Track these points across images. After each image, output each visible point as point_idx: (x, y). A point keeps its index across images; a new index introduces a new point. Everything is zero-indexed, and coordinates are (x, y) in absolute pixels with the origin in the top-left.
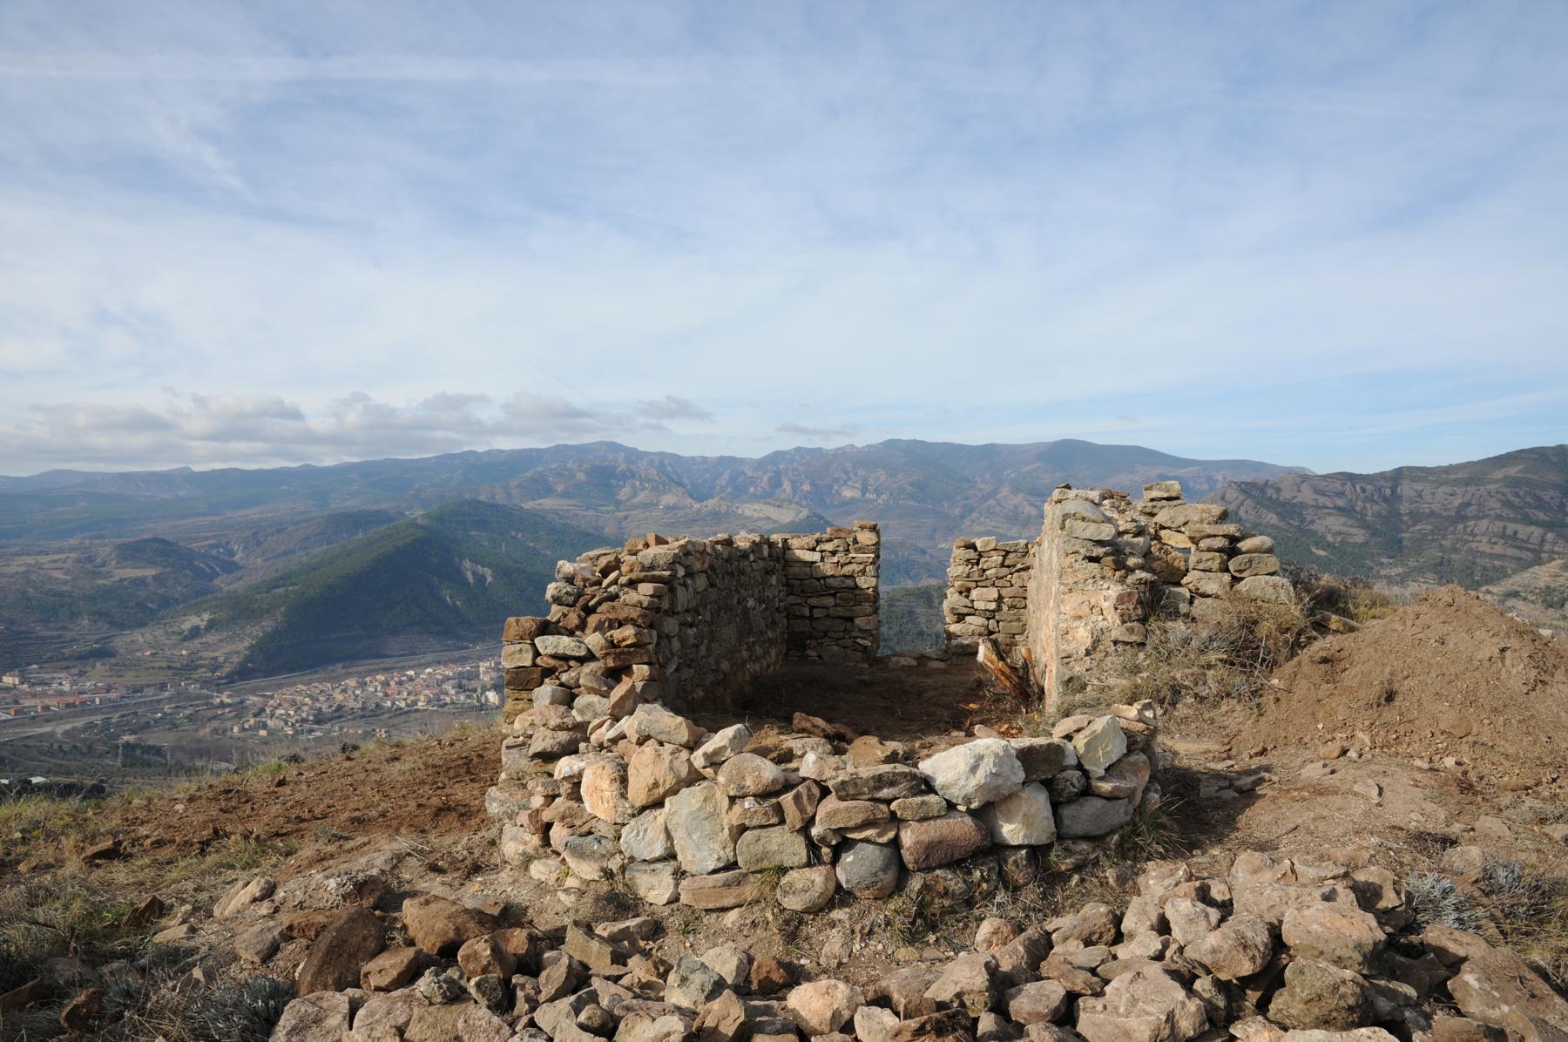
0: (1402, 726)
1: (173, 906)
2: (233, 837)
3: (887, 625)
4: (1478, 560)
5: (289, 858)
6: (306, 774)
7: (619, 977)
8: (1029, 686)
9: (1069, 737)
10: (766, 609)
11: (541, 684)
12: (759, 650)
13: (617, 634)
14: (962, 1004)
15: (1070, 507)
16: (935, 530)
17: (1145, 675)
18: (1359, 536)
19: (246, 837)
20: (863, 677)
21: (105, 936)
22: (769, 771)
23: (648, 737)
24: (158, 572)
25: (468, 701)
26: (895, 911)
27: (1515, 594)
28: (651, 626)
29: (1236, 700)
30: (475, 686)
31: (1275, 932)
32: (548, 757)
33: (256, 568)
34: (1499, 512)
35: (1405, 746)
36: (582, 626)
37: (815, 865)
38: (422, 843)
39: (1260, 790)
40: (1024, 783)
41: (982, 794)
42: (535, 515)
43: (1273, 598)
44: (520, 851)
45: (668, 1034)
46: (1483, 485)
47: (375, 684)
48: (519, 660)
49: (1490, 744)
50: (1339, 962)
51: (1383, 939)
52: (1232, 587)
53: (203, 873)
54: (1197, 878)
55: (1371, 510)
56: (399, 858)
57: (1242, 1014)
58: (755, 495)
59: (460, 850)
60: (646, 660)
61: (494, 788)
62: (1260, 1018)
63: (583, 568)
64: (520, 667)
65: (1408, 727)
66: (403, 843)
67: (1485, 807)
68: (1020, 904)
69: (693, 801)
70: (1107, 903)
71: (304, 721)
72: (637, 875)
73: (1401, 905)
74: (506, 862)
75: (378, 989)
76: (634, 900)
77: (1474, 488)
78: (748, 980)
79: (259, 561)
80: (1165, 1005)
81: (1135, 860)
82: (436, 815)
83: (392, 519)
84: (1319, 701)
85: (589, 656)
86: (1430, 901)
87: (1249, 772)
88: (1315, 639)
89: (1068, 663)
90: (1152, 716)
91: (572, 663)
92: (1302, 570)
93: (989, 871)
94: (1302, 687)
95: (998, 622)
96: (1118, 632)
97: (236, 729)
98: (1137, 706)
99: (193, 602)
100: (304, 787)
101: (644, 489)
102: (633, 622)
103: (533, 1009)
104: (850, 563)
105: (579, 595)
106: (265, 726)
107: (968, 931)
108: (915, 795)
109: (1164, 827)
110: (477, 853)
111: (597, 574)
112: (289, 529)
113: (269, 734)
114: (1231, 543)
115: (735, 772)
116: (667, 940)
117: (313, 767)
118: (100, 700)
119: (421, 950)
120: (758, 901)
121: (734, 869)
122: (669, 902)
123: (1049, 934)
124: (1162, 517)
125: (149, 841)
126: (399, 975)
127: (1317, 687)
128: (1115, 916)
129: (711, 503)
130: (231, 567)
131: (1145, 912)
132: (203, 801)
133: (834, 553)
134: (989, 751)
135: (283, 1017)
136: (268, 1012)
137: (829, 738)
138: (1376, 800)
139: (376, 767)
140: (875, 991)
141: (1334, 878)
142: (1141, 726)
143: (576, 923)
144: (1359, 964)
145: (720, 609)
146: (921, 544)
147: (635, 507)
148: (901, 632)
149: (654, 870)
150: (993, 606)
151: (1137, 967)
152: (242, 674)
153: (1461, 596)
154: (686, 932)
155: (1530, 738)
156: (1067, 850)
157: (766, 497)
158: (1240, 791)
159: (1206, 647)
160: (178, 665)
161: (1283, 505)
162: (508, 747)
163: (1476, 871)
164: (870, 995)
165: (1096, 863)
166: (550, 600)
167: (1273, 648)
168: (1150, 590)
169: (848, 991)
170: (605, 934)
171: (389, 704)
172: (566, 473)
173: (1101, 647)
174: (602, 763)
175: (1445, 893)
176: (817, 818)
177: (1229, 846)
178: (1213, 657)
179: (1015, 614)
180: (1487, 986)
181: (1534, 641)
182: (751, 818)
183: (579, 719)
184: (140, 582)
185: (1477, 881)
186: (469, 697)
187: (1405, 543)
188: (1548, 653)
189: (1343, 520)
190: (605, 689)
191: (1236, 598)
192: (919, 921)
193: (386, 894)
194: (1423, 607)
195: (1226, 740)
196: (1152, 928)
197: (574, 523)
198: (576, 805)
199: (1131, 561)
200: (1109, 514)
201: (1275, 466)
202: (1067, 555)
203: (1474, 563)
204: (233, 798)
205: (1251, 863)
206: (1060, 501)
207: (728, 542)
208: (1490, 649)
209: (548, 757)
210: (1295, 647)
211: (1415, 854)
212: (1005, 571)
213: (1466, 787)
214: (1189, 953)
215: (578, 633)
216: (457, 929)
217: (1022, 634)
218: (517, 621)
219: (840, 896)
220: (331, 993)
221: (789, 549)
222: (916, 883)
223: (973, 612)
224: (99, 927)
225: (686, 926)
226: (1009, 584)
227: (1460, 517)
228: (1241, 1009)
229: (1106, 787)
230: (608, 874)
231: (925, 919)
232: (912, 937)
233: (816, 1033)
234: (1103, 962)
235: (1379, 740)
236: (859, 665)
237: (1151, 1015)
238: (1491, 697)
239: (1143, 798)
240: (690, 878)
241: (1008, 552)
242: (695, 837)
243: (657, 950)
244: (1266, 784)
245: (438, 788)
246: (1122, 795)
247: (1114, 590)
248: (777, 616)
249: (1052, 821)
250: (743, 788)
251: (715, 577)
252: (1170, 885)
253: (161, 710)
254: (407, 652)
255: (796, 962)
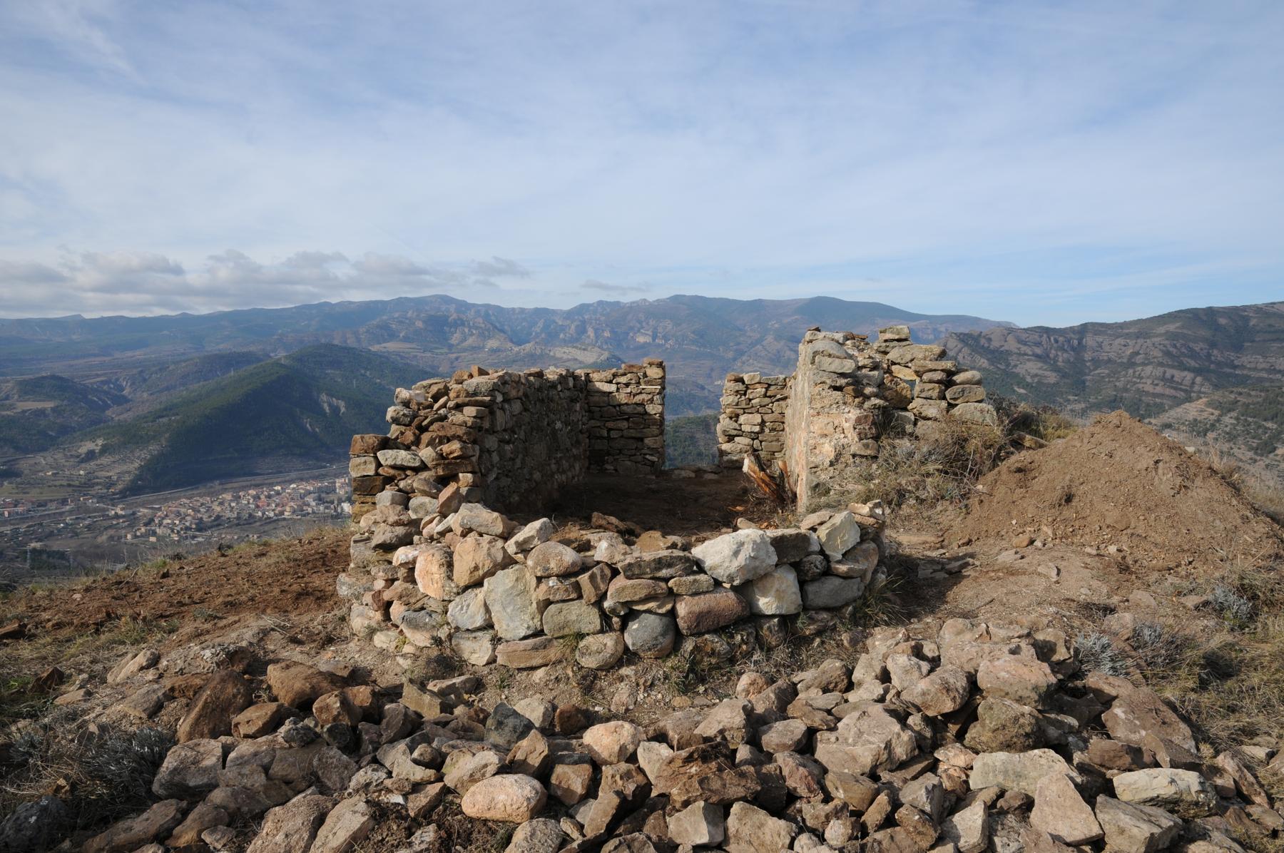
0: (1077, 522)
1: (71, 675)
2: (123, 619)
3: (672, 448)
4: (1143, 398)
5: (171, 635)
6: (187, 568)
7: (447, 723)
8: (785, 491)
9: (814, 529)
10: (572, 430)
11: (383, 489)
12: (565, 464)
13: (446, 448)
14: (724, 738)
15: (819, 345)
16: (712, 370)
17: (877, 481)
18: (1052, 378)
19: (134, 619)
20: (650, 486)
21: (13, 701)
22: (569, 556)
23: (471, 530)
24: (57, 404)
25: (327, 511)
26: (672, 667)
27: (1168, 426)
28: (474, 442)
29: (948, 502)
30: (332, 498)
31: (972, 680)
32: (388, 548)
33: (143, 402)
34: (1160, 360)
35: (1079, 537)
36: (417, 442)
37: (607, 632)
38: (284, 621)
39: (965, 572)
40: (777, 565)
41: (743, 574)
42: (381, 356)
43: (981, 420)
44: (366, 625)
45: (486, 766)
46: (1149, 338)
47: (248, 497)
48: (364, 470)
49: (1144, 535)
50: (1020, 700)
51: (1054, 682)
52: (948, 412)
53: (98, 648)
54: (913, 640)
55: (1062, 357)
56: (264, 633)
57: (944, 742)
58: (564, 340)
59: (316, 626)
60: (470, 470)
61: (344, 575)
62: (958, 745)
63: (418, 394)
64: (364, 476)
65: (1082, 522)
66: (268, 621)
67: (1138, 583)
68: (772, 662)
69: (507, 581)
70: (842, 660)
71: (188, 529)
72: (462, 642)
73: (1070, 658)
74: (354, 635)
75: (247, 736)
76: (459, 661)
77: (1142, 340)
78: (552, 724)
79: (145, 395)
80: (884, 736)
81: (865, 626)
82: (297, 599)
83: (259, 360)
84: (1014, 502)
85: (423, 466)
86: (1092, 654)
87: (957, 559)
88: (1012, 453)
89: (815, 472)
90: (881, 513)
91: (408, 472)
92: (1004, 399)
93: (748, 635)
94: (1001, 491)
95: (761, 442)
96: (856, 448)
97: (129, 536)
98: (870, 505)
99: (88, 430)
100: (185, 578)
101: (472, 334)
102: (459, 438)
103: (376, 749)
104: (641, 393)
105: (415, 416)
106: (154, 533)
107: (731, 683)
108: (688, 575)
109: (889, 601)
110: (330, 628)
111: (430, 399)
112: (170, 368)
113: (158, 540)
114: (948, 376)
115: (541, 557)
116: (486, 694)
117: (193, 563)
118: (9, 513)
119: (282, 705)
120: (560, 662)
121: (541, 636)
122: (488, 663)
123: (795, 685)
124: (893, 355)
125: (50, 624)
126: (264, 724)
127: (1013, 491)
128: (848, 669)
129: (528, 347)
130: (121, 400)
131: (871, 666)
132: (98, 591)
133: (627, 385)
134: (748, 539)
135: (166, 760)
136: (154, 756)
137: (621, 533)
138: (1055, 578)
139: (246, 561)
140: (655, 730)
141: (1019, 637)
142: (872, 520)
143: (411, 681)
144: (1036, 702)
145: (532, 429)
146: (701, 381)
147: (465, 350)
148: (684, 453)
149: (475, 638)
150: (757, 429)
151: (863, 708)
152: (133, 490)
153: (1127, 420)
154: (502, 687)
155: (1174, 531)
156: (811, 618)
157: (574, 341)
158: (950, 573)
159: (926, 460)
160: (77, 483)
161: (993, 352)
162: (356, 542)
163: (1127, 631)
164: (651, 733)
165: (834, 629)
166: (390, 420)
167: (979, 460)
168: (883, 414)
169: (633, 729)
170: (436, 690)
171: (260, 514)
172: (407, 321)
173: (843, 460)
174: (432, 551)
175: (1104, 648)
176: (609, 594)
177: (940, 615)
178: (931, 467)
179: (775, 436)
180: (1131, 717)
181: (1180, 455)
182: (555, 594)
183: (414, 517)
184: (41, 413)
185: (1128, 639)
186: (327, 508)
187: (1087, 384)
188: (1191, 465)
189: (1040, 365)
190: (435, 491)
191: (951, 421)
192: (691, 676)
193: (254, 661)
194: (1097, 428)
195: (940, 534)
196: (877, 678)
197: (414, 363)
198: (411, 586)
199: (868, 390)
200: (850, 352)
201: (987, 321)
202: (816, 385)
203: (1140, 400)
204: (126, 589)
205: (955, 627)
206: (811, 341)
207: (540, 375)
208: (1147, 461)
209: (388, 548)
210: (996, 460)
211: (1083, 620)
212: (767, 400)
213: (1124, 568)
214: (905, 696)
215: (413, 448)
216: (313, 687)
217: (780, 451)
218: (362, 438)
219: (627, 656)
220: (207, 740)
221: (590, 382)
222: (689, 645)
223: (741, 433)
224: (6, 694)
225: (502, 682)
226: (770, 411)
227: (1131, 364)
228: (944, 738)
229: (843, 568)
230: (438, 641)
231: (696, 675)
232: (686, 688)
233: (606, 763)
234: (837, 704)
235: (1059, 533)
236: (649, 477)
237: (873, 744)
238: (1146, 499)
239: (872, 578)
240: (505, 643)
241: (770, 385)
242: (509, 610)
243: (479, 702)
244: (970, 567)
245: (299, 577)
246: (855, 575)
247: (854, 414)
248: (581, 436)
249: (799, 595)
250: (547, 570)
251: (528, 403)
252: (892, 644)
253: (64, 521)
254: (274, 471)
255: (591, 709)
